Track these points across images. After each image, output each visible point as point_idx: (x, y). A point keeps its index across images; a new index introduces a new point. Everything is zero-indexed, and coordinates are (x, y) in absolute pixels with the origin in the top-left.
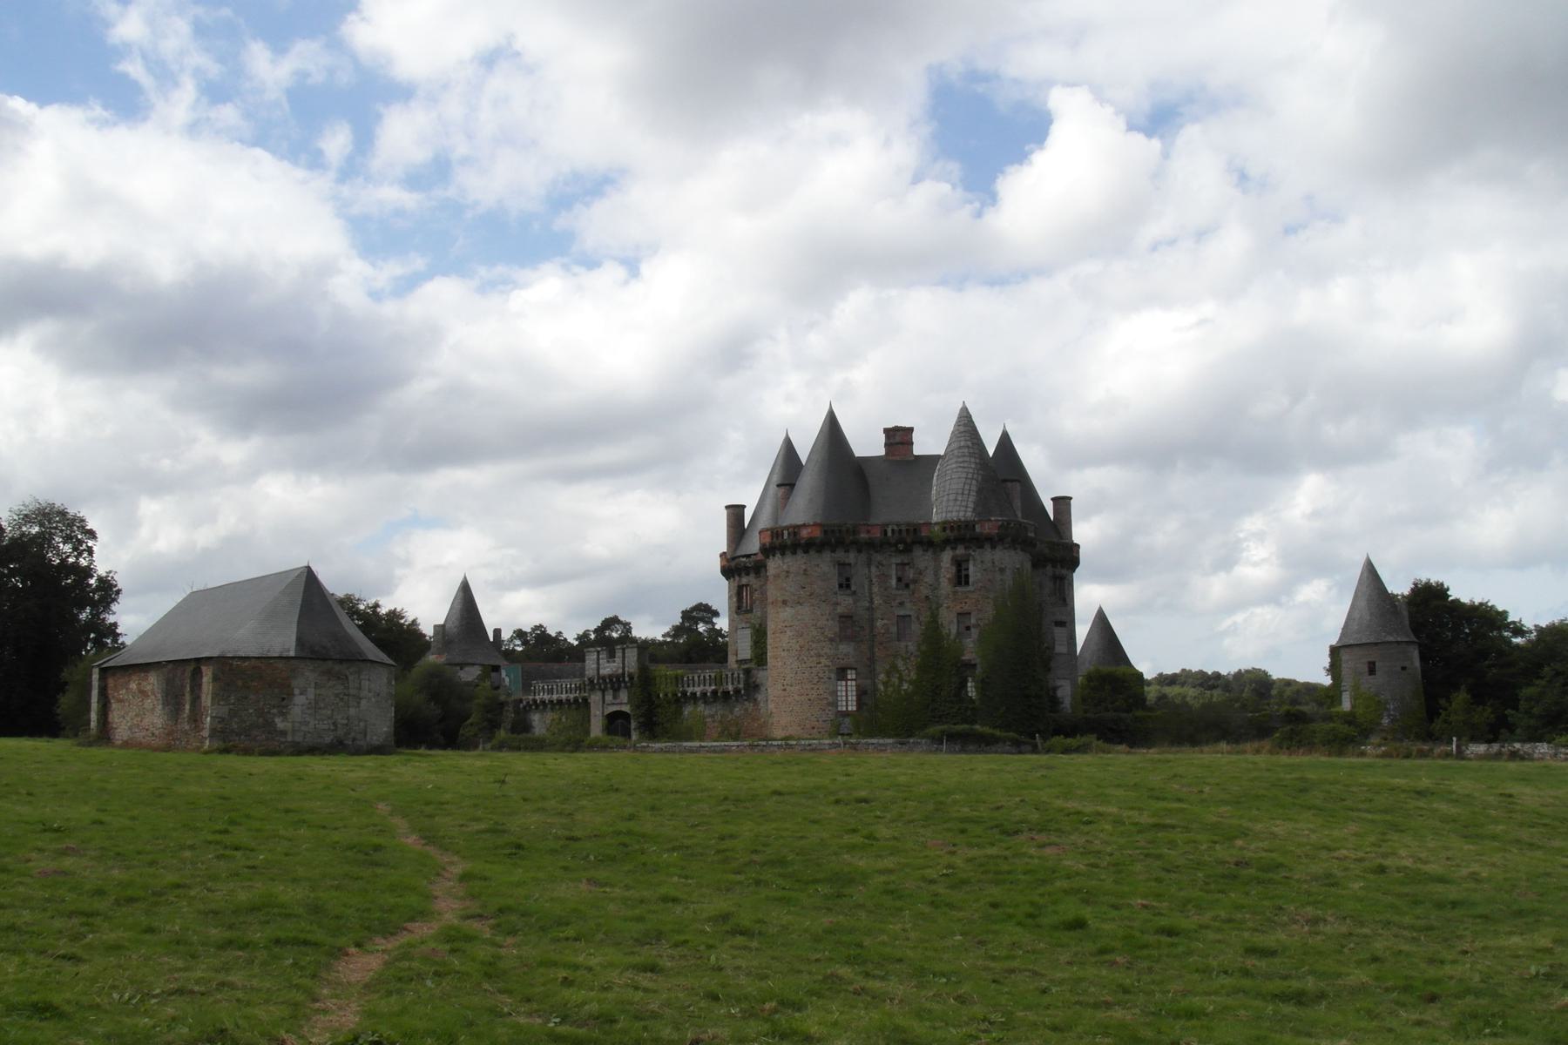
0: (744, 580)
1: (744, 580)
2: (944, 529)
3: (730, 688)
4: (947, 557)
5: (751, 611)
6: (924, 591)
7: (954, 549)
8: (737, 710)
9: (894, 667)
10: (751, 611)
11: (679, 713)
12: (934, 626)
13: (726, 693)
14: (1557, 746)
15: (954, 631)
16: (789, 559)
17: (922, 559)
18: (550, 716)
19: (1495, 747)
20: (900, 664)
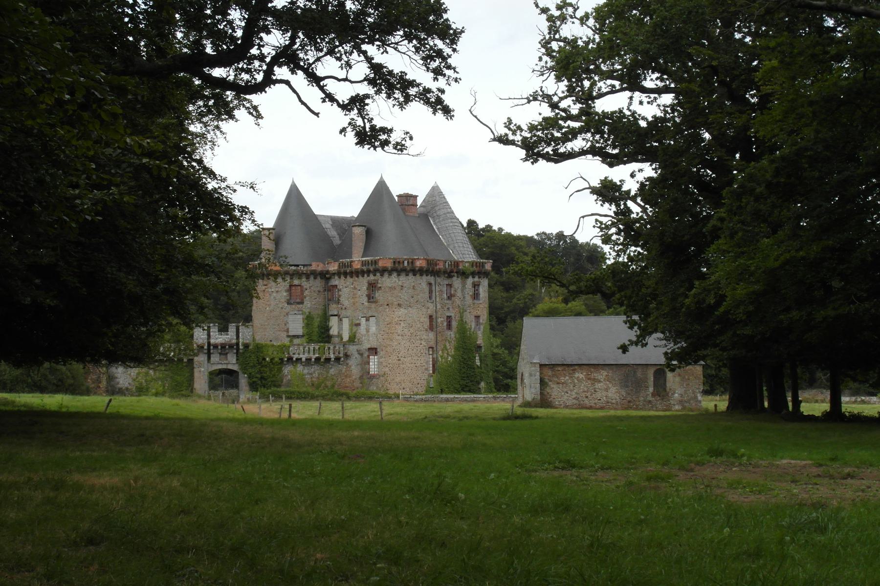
0: (296, 282)
1: (296, 282)
2: (472, 266)
3: (332, 356)
4: (470, 281)
5: (302, 303)
6: (458, 302)
7: (473, 277)
8: (332, 371)
9: (445, 346)
10: (302, 303)
11: (280, 370)
12: (462, 323)
13: (328, 360)
14: (150, 369)
15: (473, 327)
16: (403, 278)
17: (457, 282)
18: (845, 399)
19: (853, 399)
20: (448, 345)
